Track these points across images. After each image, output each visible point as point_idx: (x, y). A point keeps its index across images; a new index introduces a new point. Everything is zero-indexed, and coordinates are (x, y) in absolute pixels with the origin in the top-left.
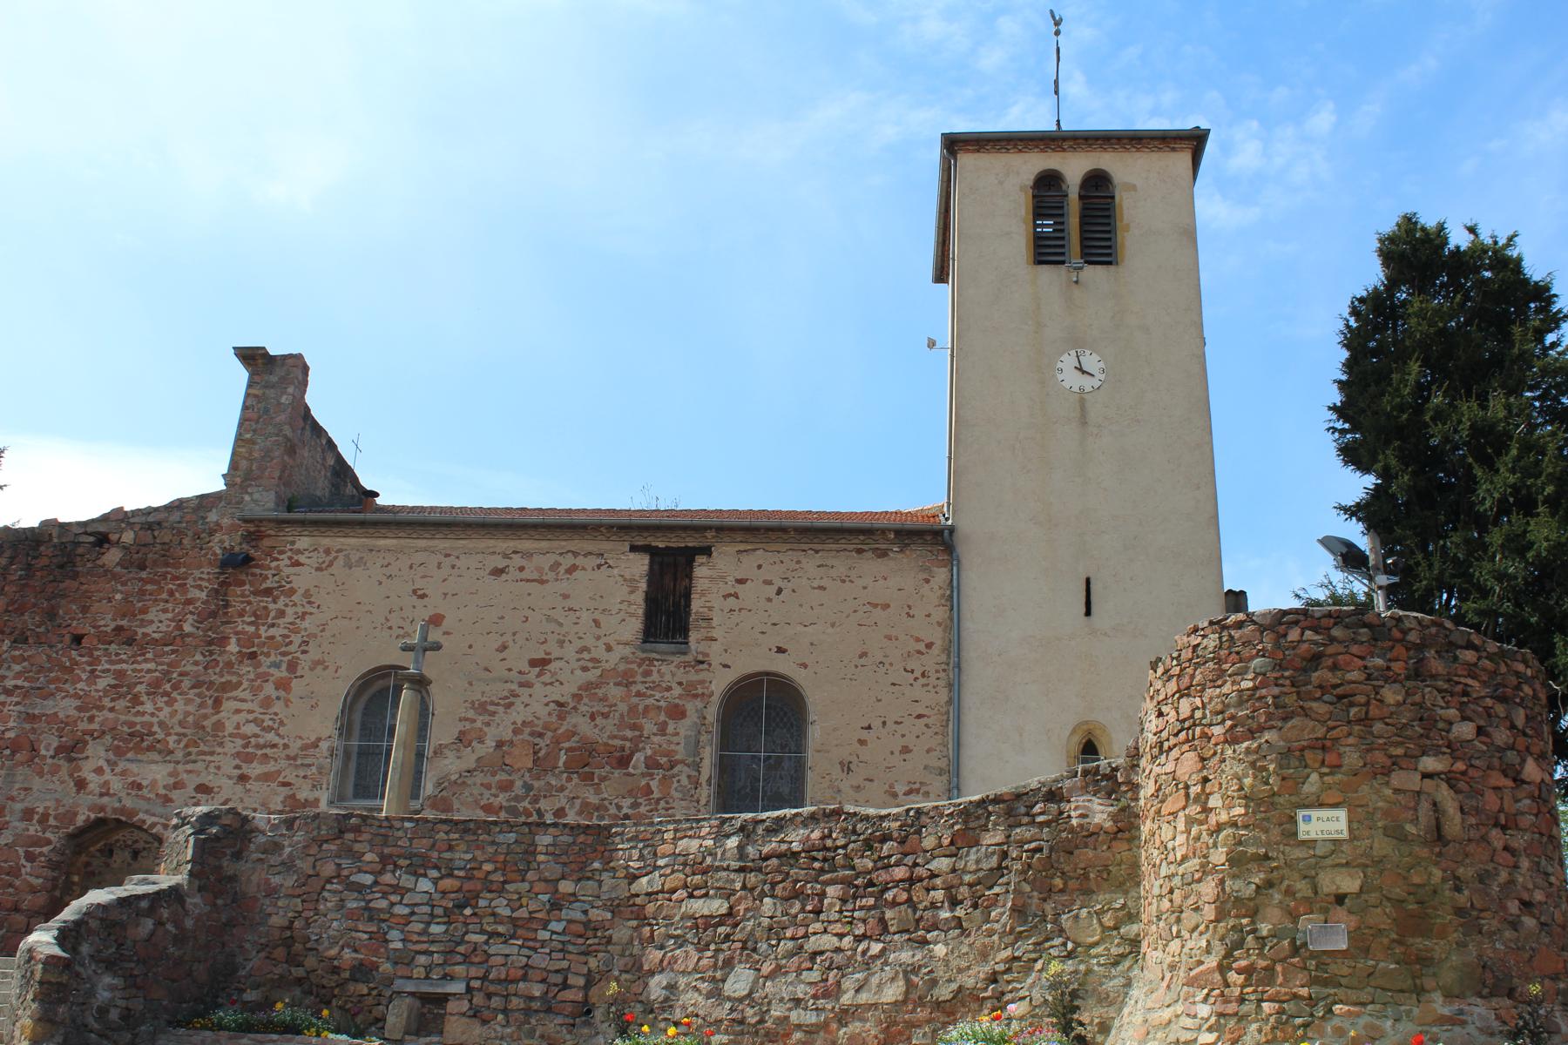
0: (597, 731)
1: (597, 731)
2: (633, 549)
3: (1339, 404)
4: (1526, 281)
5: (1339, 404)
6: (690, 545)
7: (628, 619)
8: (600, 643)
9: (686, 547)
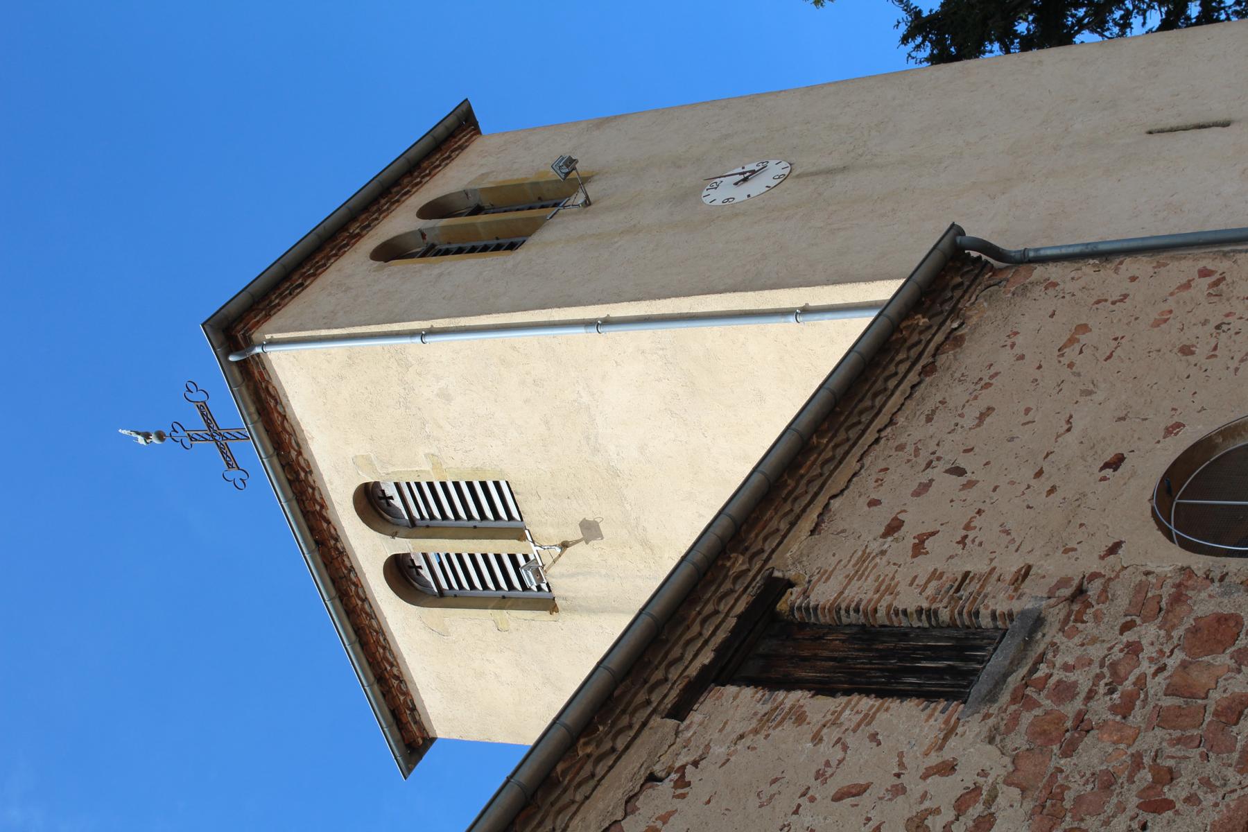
0: (1209, 799)
1: (1209, 799)
2: (680, 711)
3: (925, 14)
4: (728, 683)
5: (925, 14)
6: (740, 607)
7: (875, 727)
8: (916, 787)
9: (739, 617)
